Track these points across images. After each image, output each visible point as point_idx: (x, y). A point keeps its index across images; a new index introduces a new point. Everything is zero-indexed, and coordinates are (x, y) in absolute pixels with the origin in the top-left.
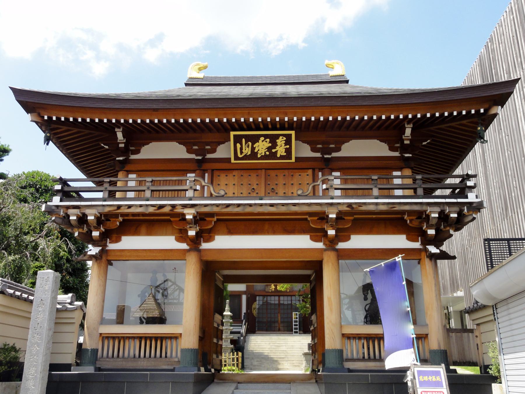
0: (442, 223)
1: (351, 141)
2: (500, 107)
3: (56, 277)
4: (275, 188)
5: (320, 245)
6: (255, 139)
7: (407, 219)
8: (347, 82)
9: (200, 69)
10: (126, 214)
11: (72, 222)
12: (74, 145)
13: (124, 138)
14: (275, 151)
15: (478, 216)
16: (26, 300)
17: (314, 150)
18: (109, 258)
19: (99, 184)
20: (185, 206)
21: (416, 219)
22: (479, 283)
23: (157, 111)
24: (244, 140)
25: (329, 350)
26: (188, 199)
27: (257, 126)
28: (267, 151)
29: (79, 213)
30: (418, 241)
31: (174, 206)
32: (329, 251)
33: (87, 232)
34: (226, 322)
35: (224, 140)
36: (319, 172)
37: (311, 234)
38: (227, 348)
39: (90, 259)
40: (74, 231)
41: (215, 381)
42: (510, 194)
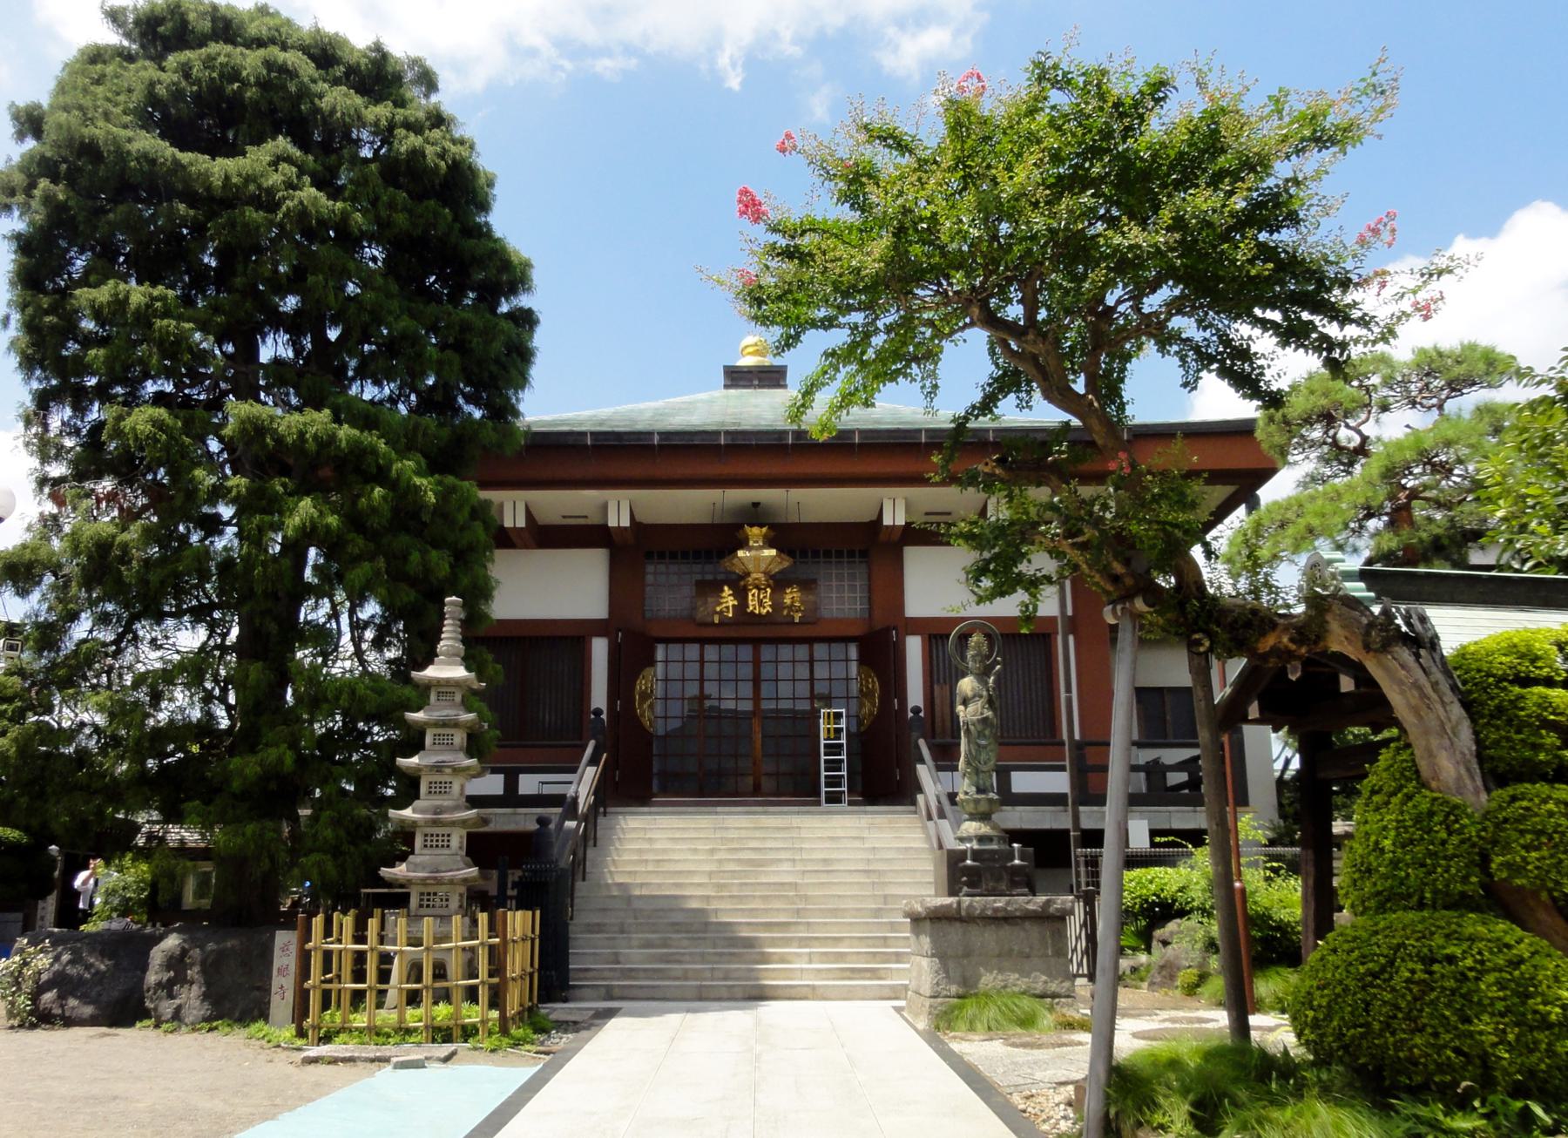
34: (436, 724)
38: (439, 882)
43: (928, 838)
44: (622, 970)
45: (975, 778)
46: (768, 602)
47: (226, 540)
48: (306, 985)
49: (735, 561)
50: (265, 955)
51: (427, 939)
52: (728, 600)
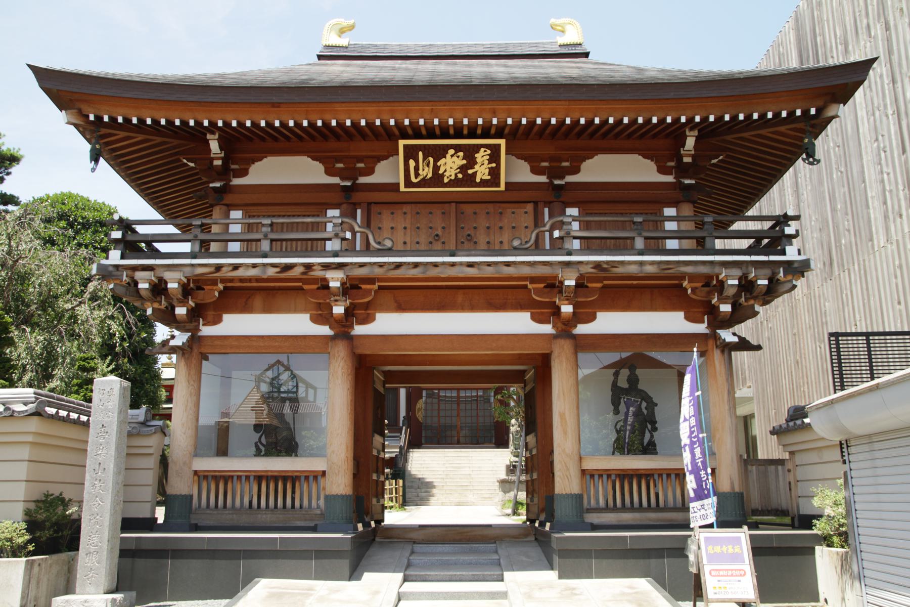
0: (743, 294)
1: (596, 157)
2: (842, 105)
3: (124, 388)
4: (473, 235)
5: (547, 329)
6: (439, 153)
7: (687, 288)
8: (586, 55)
9: (342, 32)
10: (230, 279)
11: (143, 293)
12: (180, 188)
13: (221, 150)
14: (473, 173)
15: (800, 283)
16: (77, 422)
17: (535, 171)
18: (204, 350)
19: (185, 228)
20: (327, 267)
21: (703, 286)
22: (824, 409)
23: (279, 107)
24: (421, 154)
25: (562, 496)
26: (331, 255)
27: (444, 133)
28: (459, 173)
29: (153, 278)
30: (703, 322)
31: (308, 267)
32: (561, 338)
33: (166, 307)
35: (386, 154)
36: (545, 207)
37: (533, 311)
39: (171, 351)
40: (146, 306)
41: (377, 539)
42: (838, 241)
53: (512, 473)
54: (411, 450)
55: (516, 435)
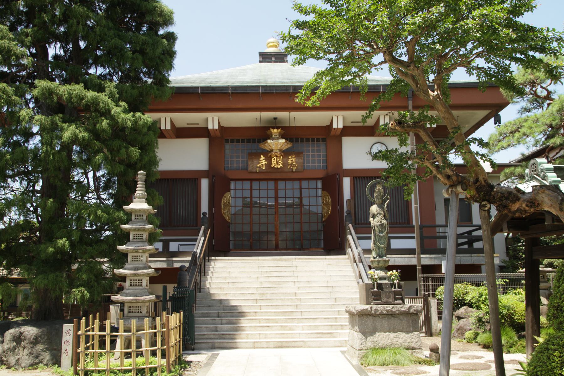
34: (135, 230)
43: (354, 271)
44: (219, 334)
45: (378, 251)
46: (281, 162)
47: (35, 142)
48: (79, 351)
49: (266, 144)
50: (59, 334)
51: (133, 329)
52: (263, 161)
53: (375, 300)
54: (213, 258)
55: (381, 232)
